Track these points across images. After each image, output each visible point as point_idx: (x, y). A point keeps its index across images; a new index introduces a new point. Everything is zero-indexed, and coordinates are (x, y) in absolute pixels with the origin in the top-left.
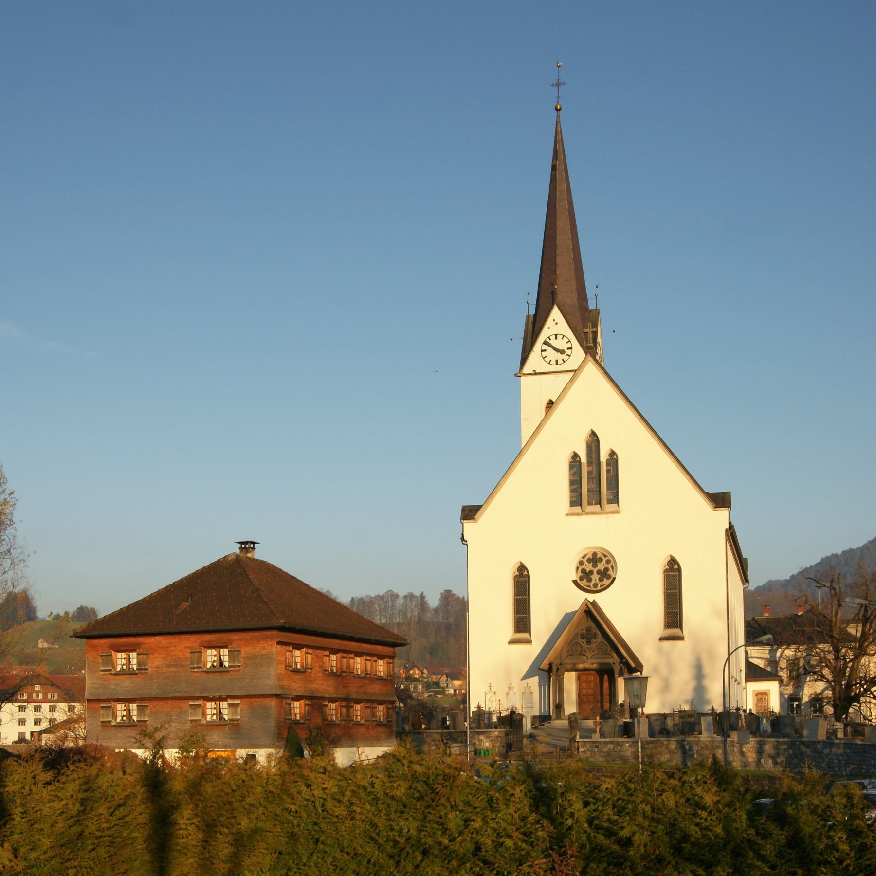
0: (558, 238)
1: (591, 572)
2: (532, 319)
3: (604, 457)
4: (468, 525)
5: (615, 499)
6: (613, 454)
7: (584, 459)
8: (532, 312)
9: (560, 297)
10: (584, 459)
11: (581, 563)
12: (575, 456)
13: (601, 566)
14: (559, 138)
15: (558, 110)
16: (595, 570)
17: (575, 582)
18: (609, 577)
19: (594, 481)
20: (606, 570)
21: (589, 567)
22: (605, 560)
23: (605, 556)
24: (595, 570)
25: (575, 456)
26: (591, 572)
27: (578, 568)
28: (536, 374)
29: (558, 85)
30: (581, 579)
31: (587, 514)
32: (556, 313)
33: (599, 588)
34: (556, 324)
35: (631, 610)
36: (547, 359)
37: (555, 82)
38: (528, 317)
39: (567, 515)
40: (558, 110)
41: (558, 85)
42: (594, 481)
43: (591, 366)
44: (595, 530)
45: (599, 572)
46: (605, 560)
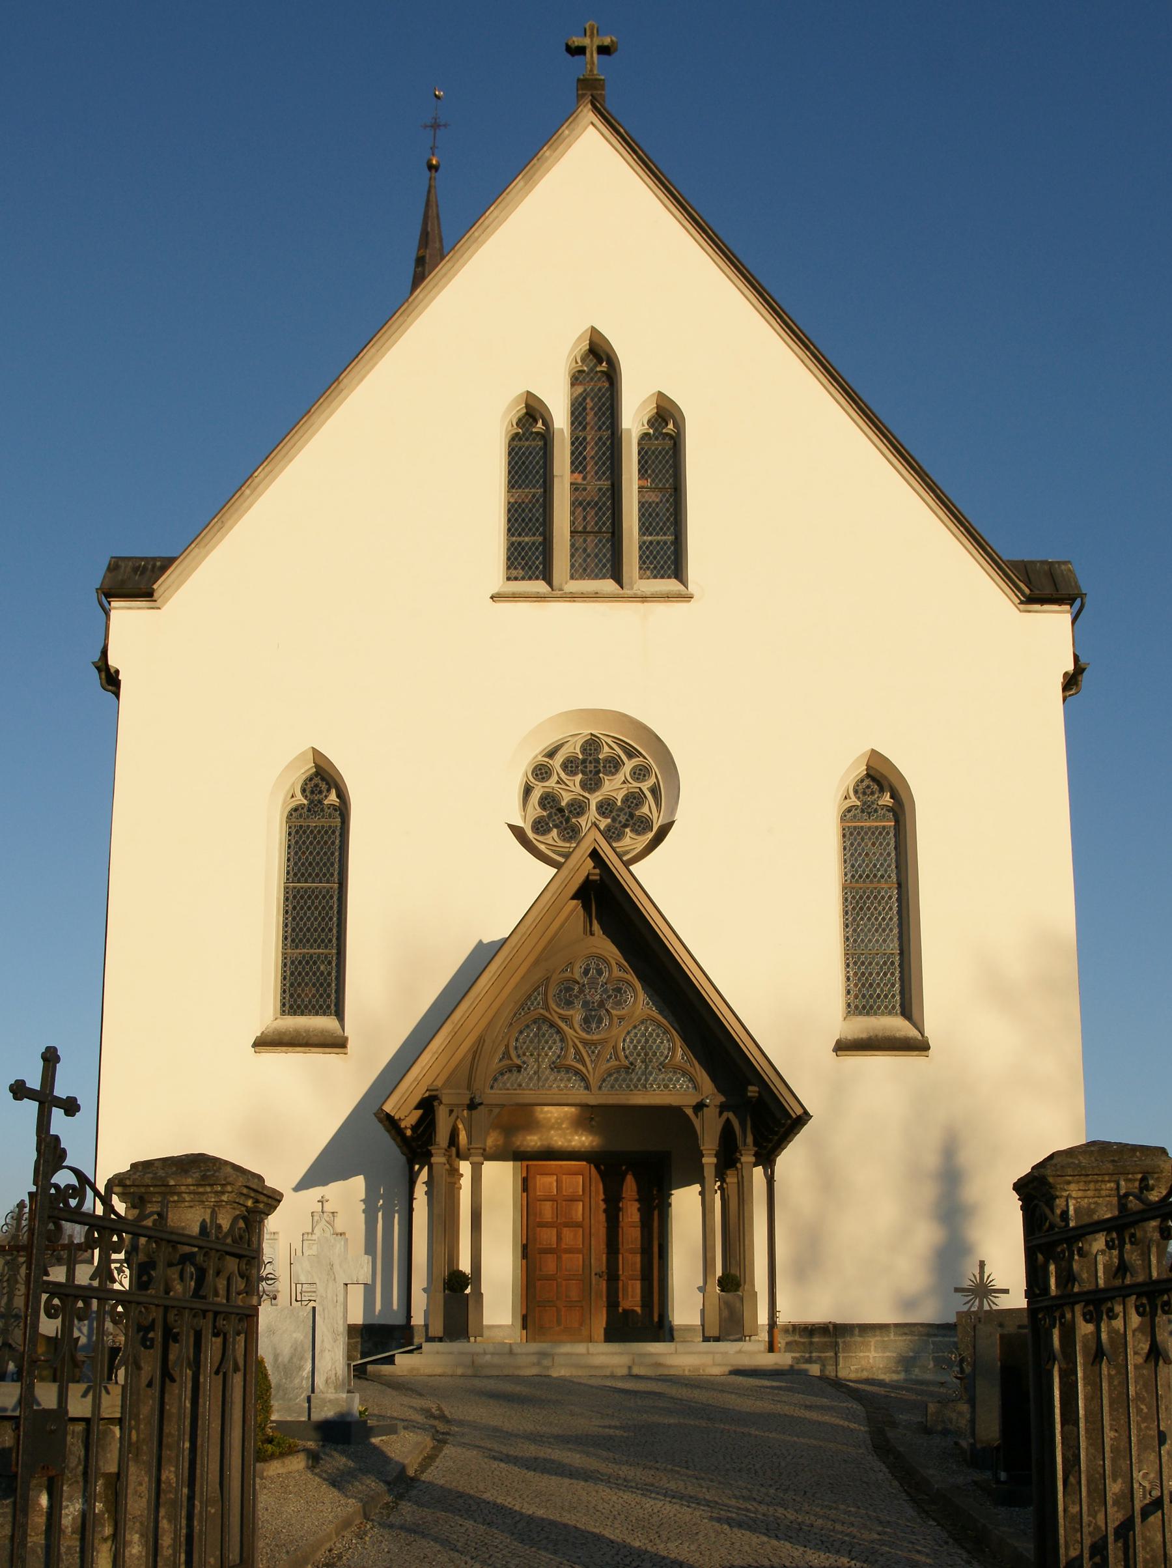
1: (579, 807)
3: (633, 418)
4: (126, 618)
5: (669, 558)
7: (561, 419)
10: (561, 419)
11: (541, 772)
12: (532, 413)
13: (615, 787)
14: (433, 198)
15: (431, 167)
17: (518, 832)
18: (642, 825)
19: (595, 495)
20: (634, 800)
21: (570, 789)
22: (629, 765)
25: (532, 413)
26: (579, 807)
27: (528, 791)
29: (435, 126)
30: (540, 826)
35: (753, 924)
41: (435, 126)
42: (595, 495)
44: (596, 654)
45: (605, 807)
46: (629, 765)
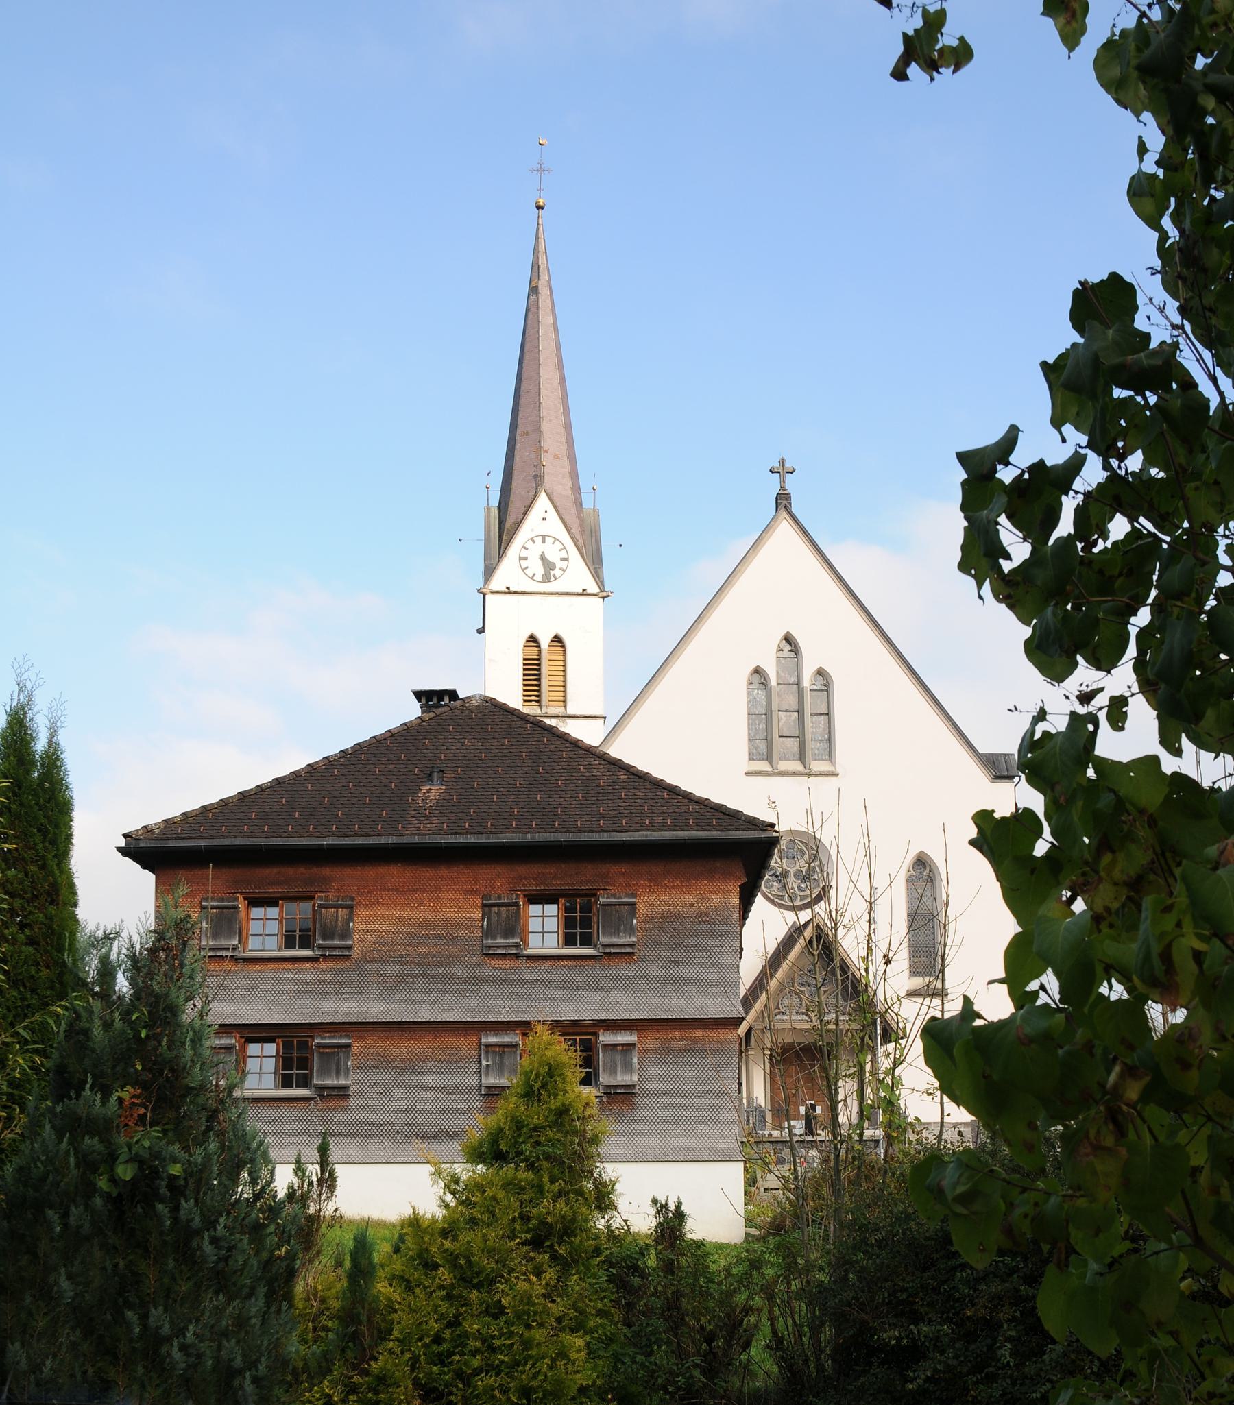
0: (544, 392)
2: (495, 512)
6: (820, 672)
8: (495, 502)
9: (548, 481)
14: (541, 248)
15: (539, 207)
16: (792, 871)
23: (810, 849)
24: (792, 871)
28: (509, 591)
31: (782, 774)
32: (543, 501)
33: (798, 903)
34: (542, 523)
36: (529, 572)
37: (536, 167)
38: (488, 508)
39: (747, 774)
40: (539, 207)
41: (541, 171)
43: (785, 527)
